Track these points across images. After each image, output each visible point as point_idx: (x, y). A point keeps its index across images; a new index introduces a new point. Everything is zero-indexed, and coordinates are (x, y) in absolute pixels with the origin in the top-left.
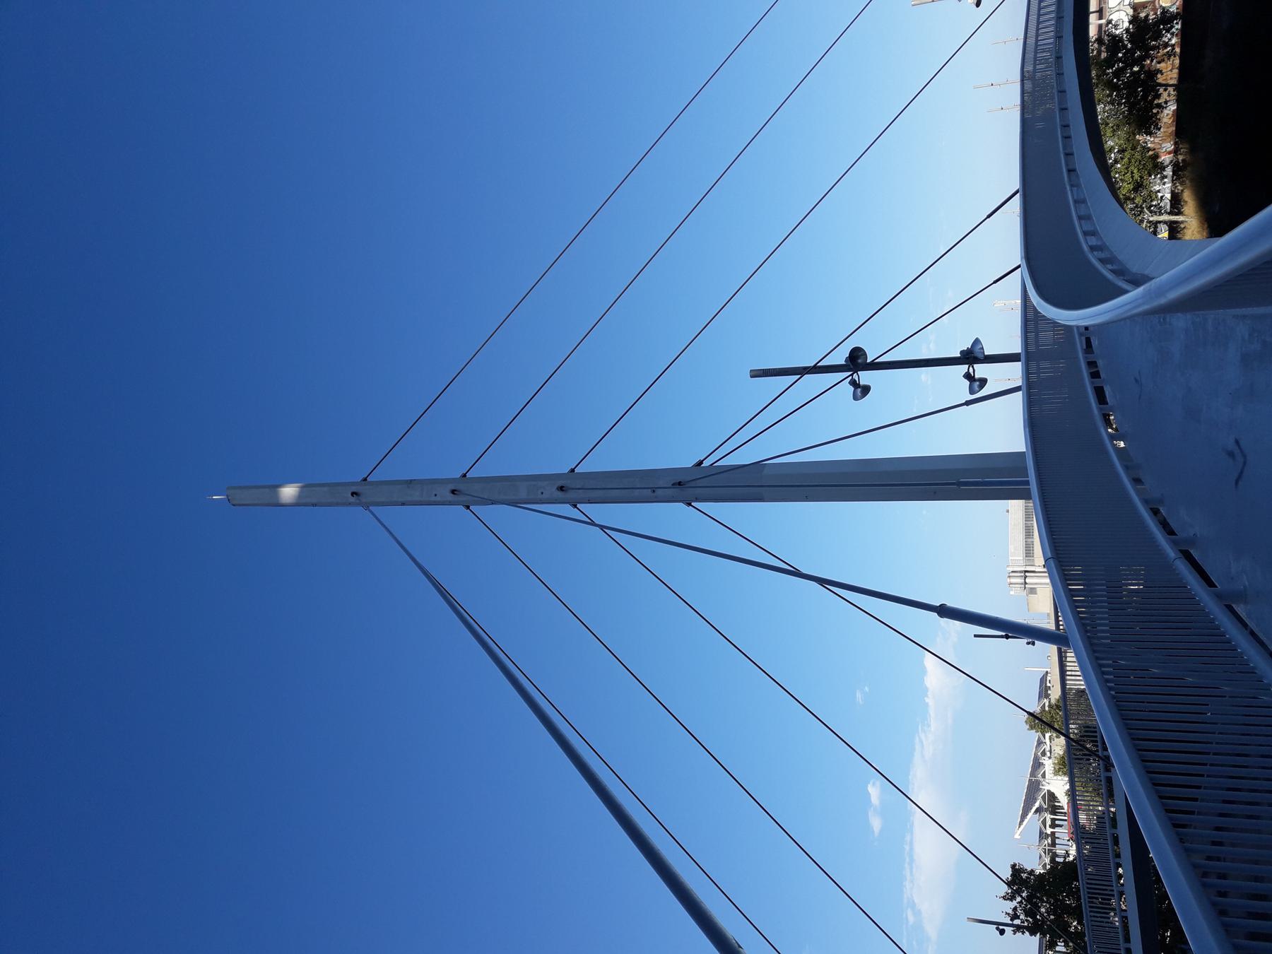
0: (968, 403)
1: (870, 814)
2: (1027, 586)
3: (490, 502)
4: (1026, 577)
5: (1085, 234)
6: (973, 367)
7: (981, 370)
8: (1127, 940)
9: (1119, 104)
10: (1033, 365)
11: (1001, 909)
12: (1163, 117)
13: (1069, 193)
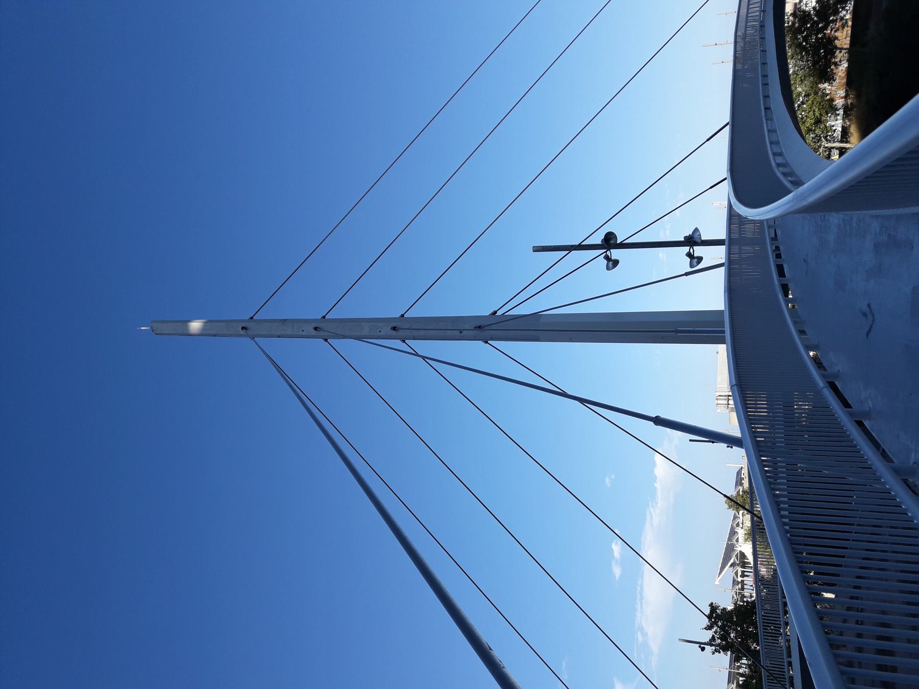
0: (687, 274)
2: (729, 406)
3: (342, 337)
4: (729, 400)
5: (774, 154)
6: (693, 248)
7: (698, 251)
8: (789, 656)
9: (807, 61)
10: (735, 249)
12: (839, 72)
13: (765, 124)
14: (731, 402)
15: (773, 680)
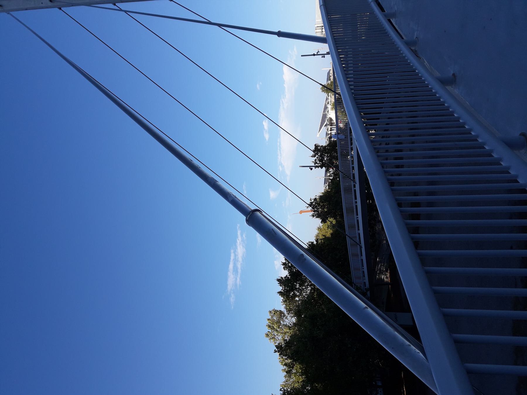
1: (264, 133)
2: (323, 33)
8: (353, 164)
11: (310, 161)
14: (324, 30)
15: (345, 177)
